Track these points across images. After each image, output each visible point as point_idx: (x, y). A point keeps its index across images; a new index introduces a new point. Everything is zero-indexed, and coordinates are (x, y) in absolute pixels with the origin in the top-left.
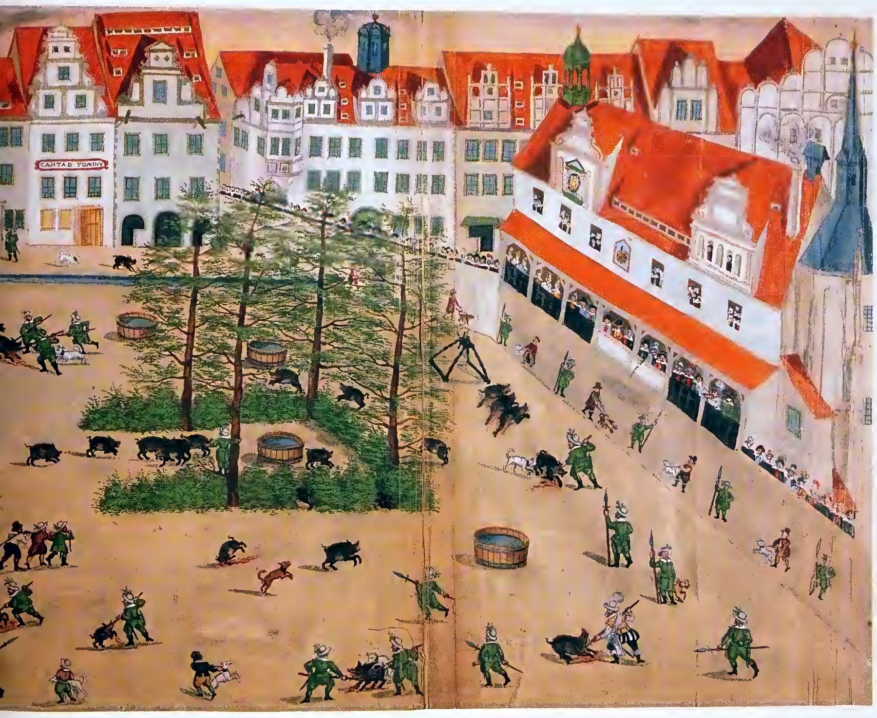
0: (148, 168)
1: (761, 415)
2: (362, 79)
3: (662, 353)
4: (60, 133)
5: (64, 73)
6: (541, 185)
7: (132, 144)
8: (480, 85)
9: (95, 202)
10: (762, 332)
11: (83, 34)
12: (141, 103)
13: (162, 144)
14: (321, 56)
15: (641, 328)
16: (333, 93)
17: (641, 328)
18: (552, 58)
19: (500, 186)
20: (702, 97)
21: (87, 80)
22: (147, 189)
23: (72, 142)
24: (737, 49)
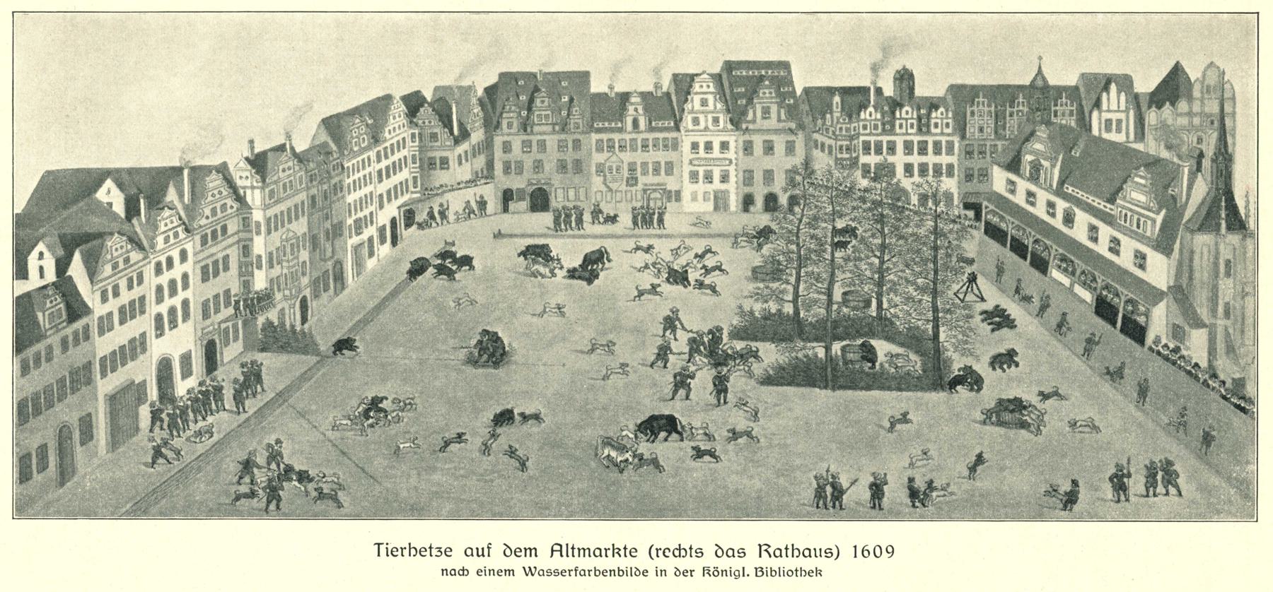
0: (760, 162)
1: (1159, 321)
2: (895, 104)
3: (1094, 280)
4: (702, 141)
5: (704, 103)
6: (1013, 177)
7: (748, 148)
8: (975, 108)
9: (723, 187)
10: (1159, 272)
11: (717, 78)
12: (754, 121)
13: (769, 148)
14: (869, 89)
15: (1080, 265)
16: (879, 116)
17: (1080, 265)
18: (1021, 88)
19: (1114, 127)
20: (1122, 116)
21: (719, 106)
22: (758, 176)
23: (709, 147)
24: (1146, 84)
